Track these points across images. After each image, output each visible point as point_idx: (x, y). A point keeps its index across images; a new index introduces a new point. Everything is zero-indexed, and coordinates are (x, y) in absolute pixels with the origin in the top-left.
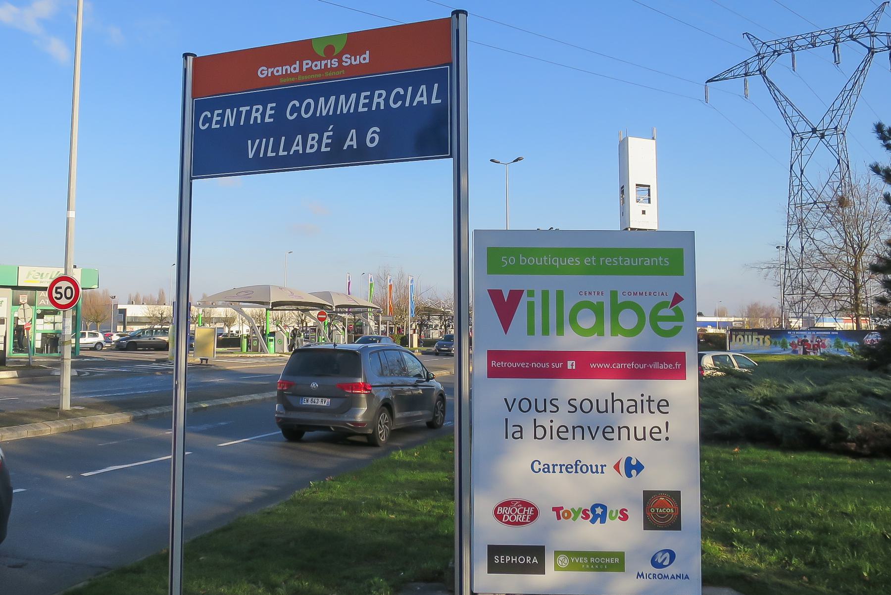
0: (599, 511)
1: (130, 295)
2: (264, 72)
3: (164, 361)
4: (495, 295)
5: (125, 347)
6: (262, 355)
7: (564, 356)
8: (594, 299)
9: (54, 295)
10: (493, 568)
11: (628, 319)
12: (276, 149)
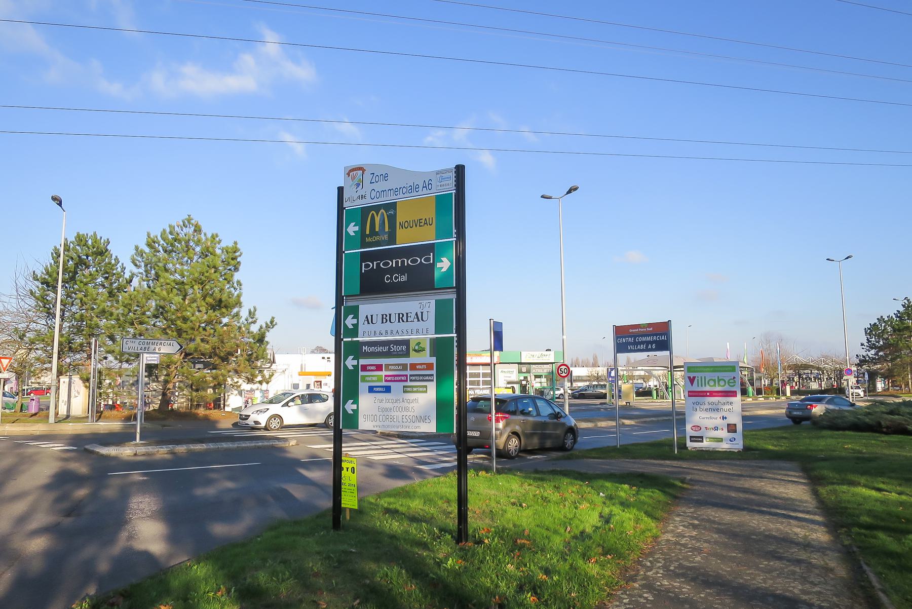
0: (716, 428)
1: (572, 359)
2: (631, 331)
3: (605, 404)
4: (689, 378)
5: (578, 396)
6: (665, 401)
7: (706, 392)
8: (713, 378)
9: (560, 372)
10: (691, 441)
11: (722, 383)
12: (634, 348)
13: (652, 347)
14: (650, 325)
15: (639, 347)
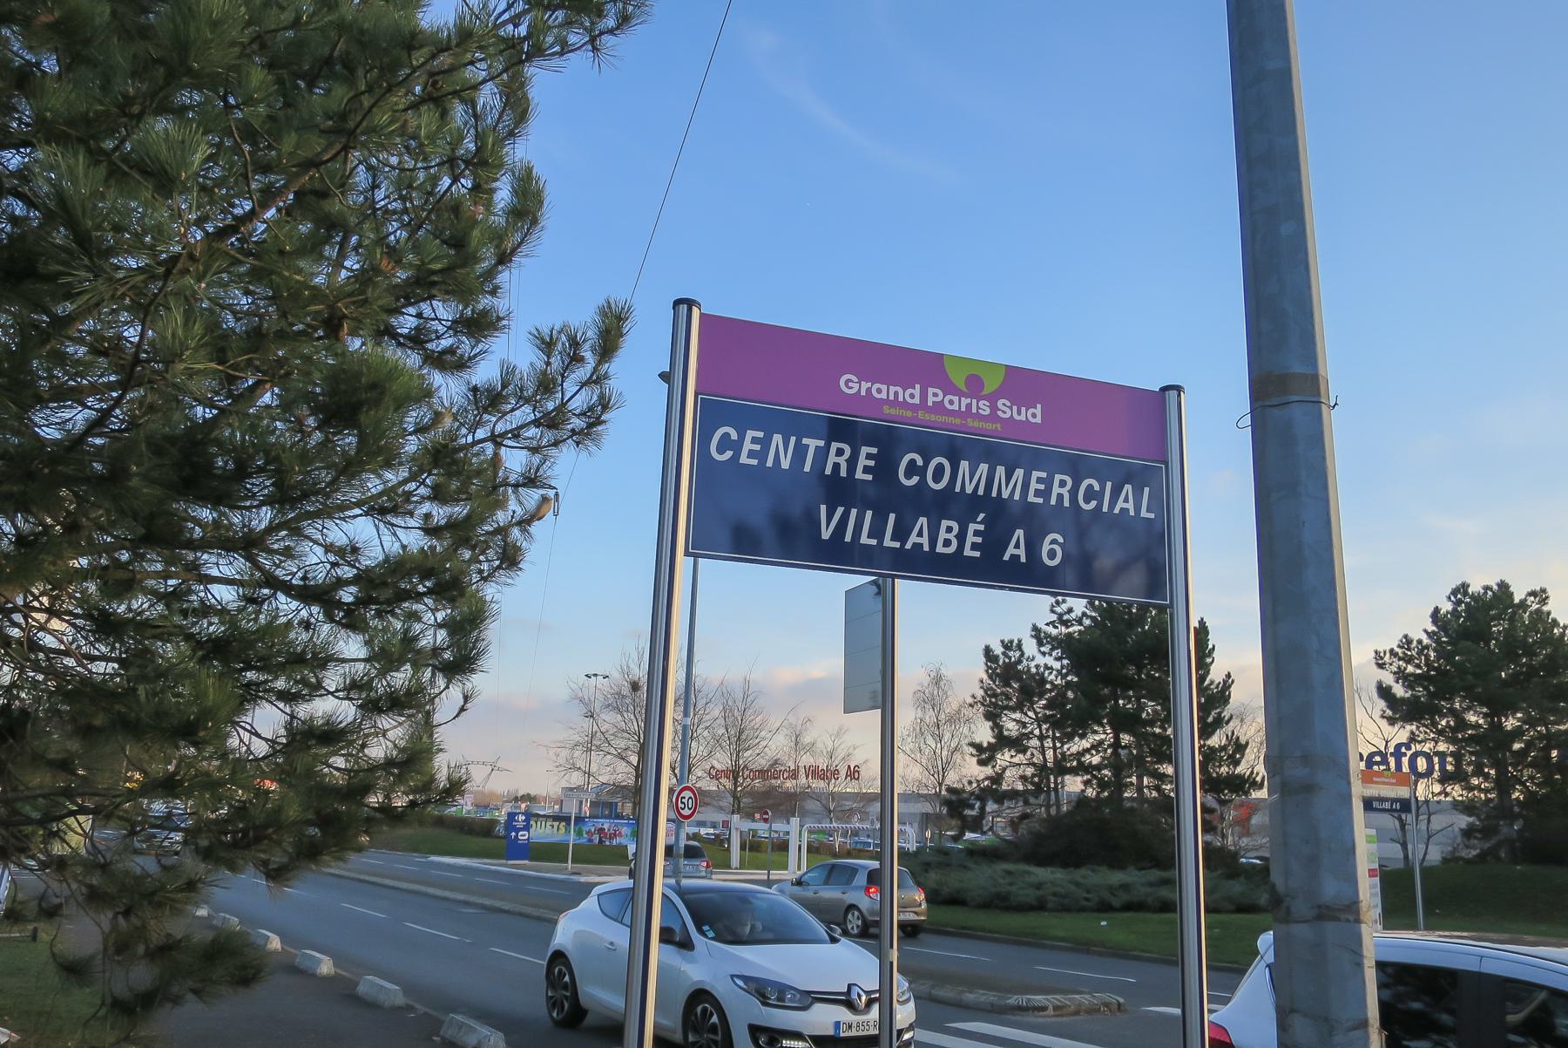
2: (850, 384)
12: (877, 532)
13: (1032, 547)
14: (1021, 383)
15: (918, 537)
